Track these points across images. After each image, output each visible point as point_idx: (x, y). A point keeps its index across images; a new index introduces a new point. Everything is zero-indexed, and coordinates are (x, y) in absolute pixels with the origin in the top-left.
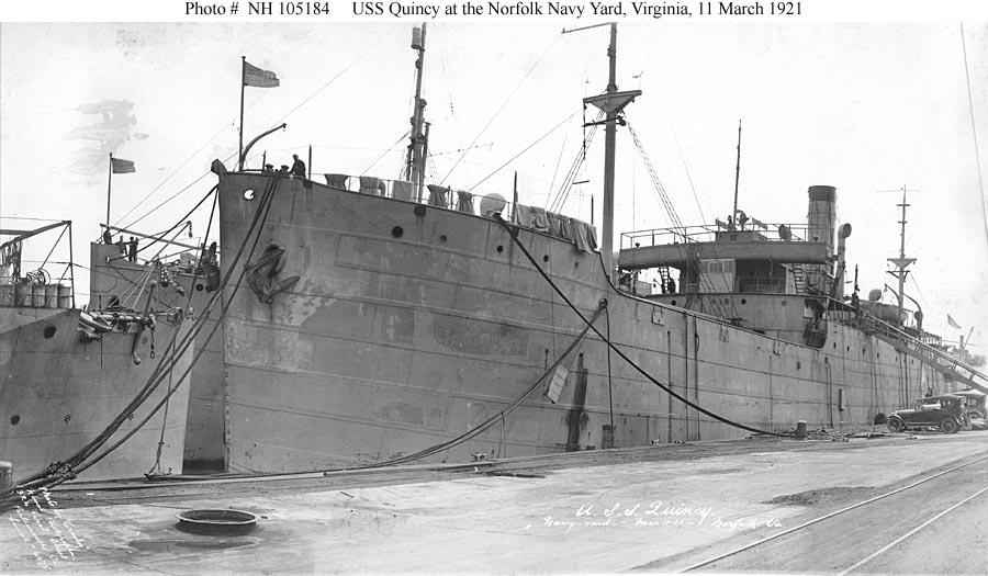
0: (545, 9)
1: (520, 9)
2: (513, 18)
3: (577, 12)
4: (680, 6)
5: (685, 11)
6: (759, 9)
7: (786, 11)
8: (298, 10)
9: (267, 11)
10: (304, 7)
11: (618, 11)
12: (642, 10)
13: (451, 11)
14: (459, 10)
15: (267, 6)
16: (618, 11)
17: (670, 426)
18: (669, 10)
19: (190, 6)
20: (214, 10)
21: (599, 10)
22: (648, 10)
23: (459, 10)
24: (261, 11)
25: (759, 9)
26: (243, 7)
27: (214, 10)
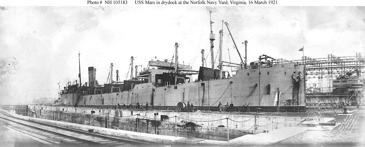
0: (206, 2)
1: (199, 3)
2: (197, 5)
3: (215, 3)
4: (157, 2)
5: (245, 3)
6: (265, 2)
7: (273, 3)
8: (119, 3)
9: (110, 3)
10: (120, 2)
11: (226, 3)
12: (233, 3)
13: (180, 3)
14: (182, 3)
15: (110, 2)
16: (226, 3)
17: (214, 121)
18: (241, 3)
19: (89, 2)
20: (95, 3)
21: (221, 3)
22: (234, 3)
23: (182, 3)
24: (108, 3)
25: (265, 2)
26: (104, 2)
27: (95, 3)
